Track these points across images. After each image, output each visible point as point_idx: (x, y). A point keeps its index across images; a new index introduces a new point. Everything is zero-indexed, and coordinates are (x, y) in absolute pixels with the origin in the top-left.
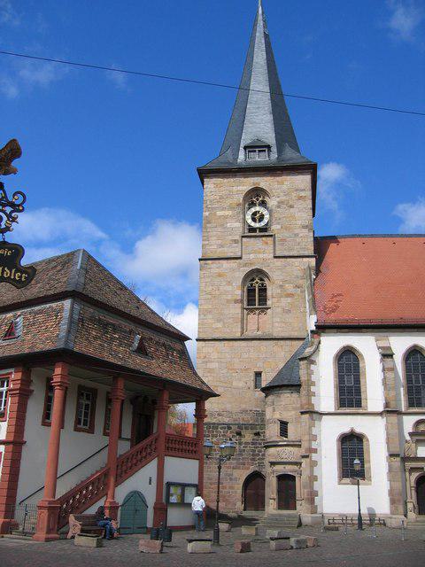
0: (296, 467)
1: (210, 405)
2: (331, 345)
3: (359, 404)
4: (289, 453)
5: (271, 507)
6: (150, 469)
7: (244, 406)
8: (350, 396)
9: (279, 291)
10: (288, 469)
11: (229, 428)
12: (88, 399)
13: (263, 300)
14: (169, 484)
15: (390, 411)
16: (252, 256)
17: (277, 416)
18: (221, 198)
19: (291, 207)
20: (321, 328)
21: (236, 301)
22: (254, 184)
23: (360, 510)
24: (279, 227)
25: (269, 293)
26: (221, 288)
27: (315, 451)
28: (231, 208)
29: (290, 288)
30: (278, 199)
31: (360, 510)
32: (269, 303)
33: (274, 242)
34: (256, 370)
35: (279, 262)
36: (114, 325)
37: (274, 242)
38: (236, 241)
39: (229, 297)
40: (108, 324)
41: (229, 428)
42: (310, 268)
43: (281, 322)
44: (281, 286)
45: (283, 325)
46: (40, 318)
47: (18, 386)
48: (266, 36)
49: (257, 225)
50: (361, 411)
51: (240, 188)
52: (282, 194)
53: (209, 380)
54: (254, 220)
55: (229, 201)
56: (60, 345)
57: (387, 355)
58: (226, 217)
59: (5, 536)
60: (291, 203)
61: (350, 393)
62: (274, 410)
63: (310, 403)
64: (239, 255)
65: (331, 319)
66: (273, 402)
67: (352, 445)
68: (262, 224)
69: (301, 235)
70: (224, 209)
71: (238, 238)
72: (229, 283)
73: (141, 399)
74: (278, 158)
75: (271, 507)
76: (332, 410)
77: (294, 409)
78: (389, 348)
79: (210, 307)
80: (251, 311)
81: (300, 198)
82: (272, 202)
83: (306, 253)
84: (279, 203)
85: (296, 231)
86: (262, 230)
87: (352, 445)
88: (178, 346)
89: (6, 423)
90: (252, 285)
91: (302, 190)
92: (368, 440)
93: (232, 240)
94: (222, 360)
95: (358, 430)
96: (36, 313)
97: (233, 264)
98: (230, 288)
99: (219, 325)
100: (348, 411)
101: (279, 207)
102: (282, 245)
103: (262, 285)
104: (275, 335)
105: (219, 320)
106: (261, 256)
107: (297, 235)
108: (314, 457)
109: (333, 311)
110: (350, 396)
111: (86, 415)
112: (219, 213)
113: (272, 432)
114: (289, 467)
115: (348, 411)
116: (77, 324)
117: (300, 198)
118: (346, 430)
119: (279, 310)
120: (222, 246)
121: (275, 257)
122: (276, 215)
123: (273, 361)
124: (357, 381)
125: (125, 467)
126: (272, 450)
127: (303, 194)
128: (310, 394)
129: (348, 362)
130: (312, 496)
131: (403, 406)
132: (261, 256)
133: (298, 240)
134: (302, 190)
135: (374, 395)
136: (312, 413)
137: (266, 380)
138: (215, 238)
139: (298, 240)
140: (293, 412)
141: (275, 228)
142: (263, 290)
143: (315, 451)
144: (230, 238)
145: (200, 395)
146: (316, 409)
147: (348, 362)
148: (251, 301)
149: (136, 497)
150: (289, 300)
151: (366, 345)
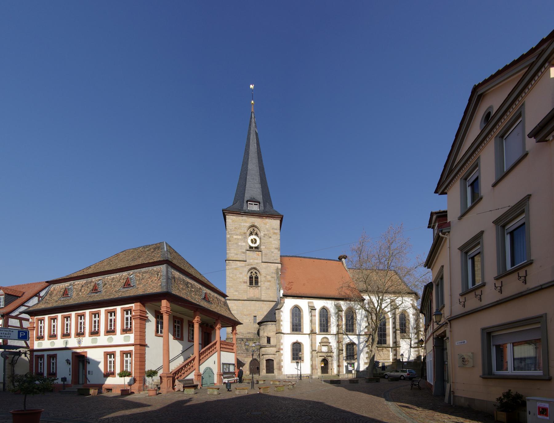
0: (274, 356)
1: (238, 327)
2: (289, 303)
3: (327, 331)
4: (273, 350)
5: (263, 371)
6: (215, 357)
7: (249, 331)
8: (296, 328)
9: (264, 279)
10: (270, 357)
11: (243, 340)
12: (178, 323)
13: (257, 283)
14: (224, 364)
15: (312, 332)
16: (251, 261)
17: (266, 334)
18: (235, 228)
19: (270, 237)
20: (285, 296)
21: (245, 282)
22: (252, 223)
23: (301, 372)
24: (264, 247)
25: (259, 280)
26: (237, 275)
27: (282, 349)
28: (241, 235)
29: (269, 277)
30: (264, 233)
31: (301, 372)
32: (259, 284)
33: (262, 255)
34: (254, 315)
35: (264, 265)
36: (191, 284)
37: (262, 255)
38: (243, 253)
39: (241, 280)
40: (188, 283)
41: (243, 340)
42: (278, 268)
43: (265, 293)
44: (265, 277)
45: (266, 295)
46: (147, 276)
47: (139, 314)
48: (257, 134)
49: (253, 245)
50: (301, 333)
51: (245, 224)
52: (266, 230)
53: (239, 317)
54: (255, 240)
55: (239, 231)
56: (164, 290)
57: (312, 309)
58: (238, 239)
59: (141, 392)
60: (270, 235)
61: (324, 326)
62: (264, 332)
63: (279, 329)
64: (244, 260)
65: (289, 292)
66: (264, 329)
67: (297, 349)
68: (256, 245)
69: (274, 252)
70: (237, 235)
71: (244, 251)
72: (241, 273)
73: (205, 325)
74: (264, 210)
75: (263, 371)
76: (289, 332)
77: (273, 331)
78: (314, 307)
79: (232, 284)
80: (251, 287)
81: (274, 233)
82: (261, 234)
83: (277, 262)
84: (264, 234)
85: (272, 250)
86: (257, 248)
87: (297, 349)
88: (223, 299)
89: (134, 334)
90: (251, 275)
91: (275, 229)
92: (303, 345)
93: (238, 255)
94: (239, 310)
95: (299, 341)
96: (143, 273)
97: (242, 264)
98: (241, 276)
99: (237, 293)
100: (295, 333)
101: (264, 237)
102: (265, 256)
103: (256, 275)
104: (262, 299)
105: (236, 291)
106: (256, 261)
107: (272, 252)
108: (282, 352)
109: (290, 289)
110: (296, 328)
111: (178, 331)
112: (235, 237)
113: (264, 341)
114: (270, 356)
115: (295, 333)
116: (169, 279)
117: (274, 233)
118: (295, 341)
119: (264, 288)
120: (237, 254)
121: (262, 262)
122: (262, 241)
123: (263, 311)
124: (300, 321)
125: (202, 356)
126: (263, 349)
127: (276, 231)
128: (280, 326)
129: (296, 312)
130: (280, 368)
131: (317, 330)
132: (256, 261)
133: (273, 255)
134: (275, 229)
135: (306, 327)
136: (279, 333)
137: (259, 319)
138: (233, 250)
139: (273, 255)
140: (273, 333)
141: (262, 247)
142: (257, 278)
143: (282, 349)
144: (241, 250)
145: (234, 323)
146: (283, 332)
147: (296, 312)
148: (251, 283)
149: (209, 370)
150: (269, 283)
151: (303, 304)
